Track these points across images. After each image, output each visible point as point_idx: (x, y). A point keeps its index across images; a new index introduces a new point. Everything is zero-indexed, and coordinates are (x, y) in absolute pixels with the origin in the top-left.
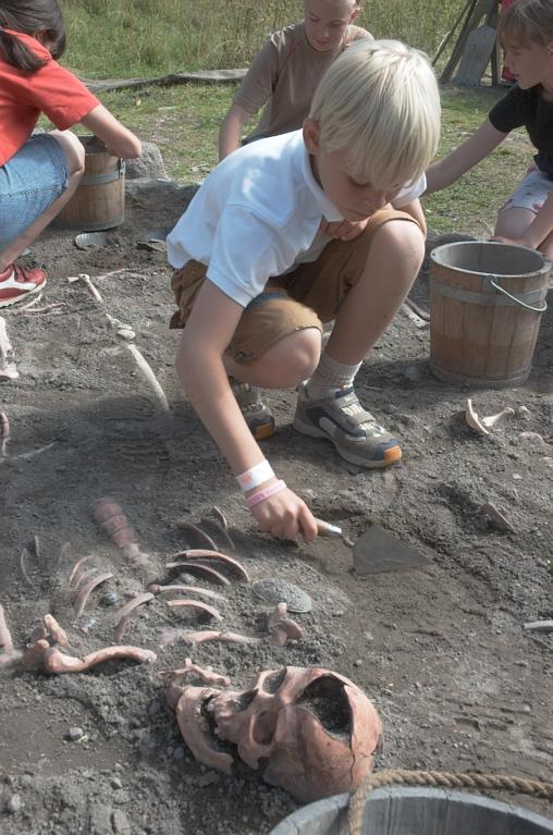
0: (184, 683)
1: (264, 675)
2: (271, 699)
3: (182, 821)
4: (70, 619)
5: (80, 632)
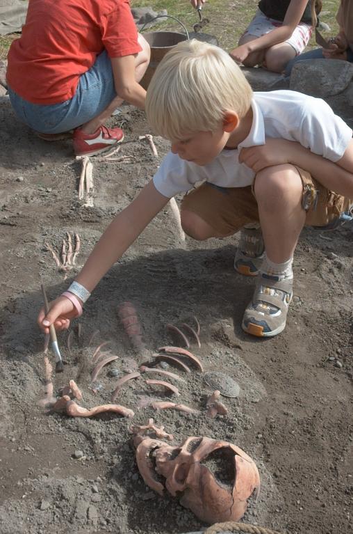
0: (145, 434)
1: (190, 439)
2: (189, 456)
3: (128, 519)
4: (88, 382)
5: (92, 392)
